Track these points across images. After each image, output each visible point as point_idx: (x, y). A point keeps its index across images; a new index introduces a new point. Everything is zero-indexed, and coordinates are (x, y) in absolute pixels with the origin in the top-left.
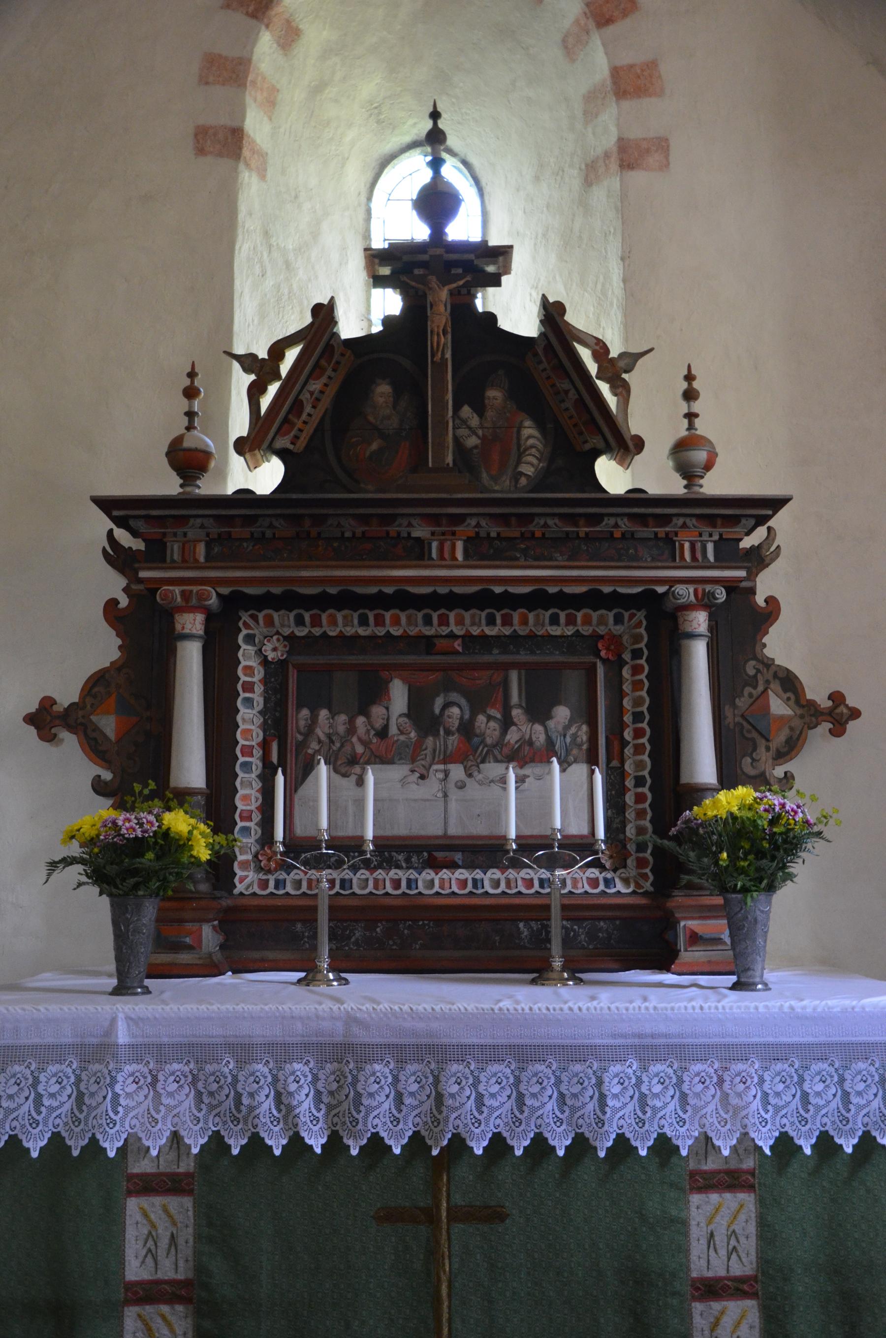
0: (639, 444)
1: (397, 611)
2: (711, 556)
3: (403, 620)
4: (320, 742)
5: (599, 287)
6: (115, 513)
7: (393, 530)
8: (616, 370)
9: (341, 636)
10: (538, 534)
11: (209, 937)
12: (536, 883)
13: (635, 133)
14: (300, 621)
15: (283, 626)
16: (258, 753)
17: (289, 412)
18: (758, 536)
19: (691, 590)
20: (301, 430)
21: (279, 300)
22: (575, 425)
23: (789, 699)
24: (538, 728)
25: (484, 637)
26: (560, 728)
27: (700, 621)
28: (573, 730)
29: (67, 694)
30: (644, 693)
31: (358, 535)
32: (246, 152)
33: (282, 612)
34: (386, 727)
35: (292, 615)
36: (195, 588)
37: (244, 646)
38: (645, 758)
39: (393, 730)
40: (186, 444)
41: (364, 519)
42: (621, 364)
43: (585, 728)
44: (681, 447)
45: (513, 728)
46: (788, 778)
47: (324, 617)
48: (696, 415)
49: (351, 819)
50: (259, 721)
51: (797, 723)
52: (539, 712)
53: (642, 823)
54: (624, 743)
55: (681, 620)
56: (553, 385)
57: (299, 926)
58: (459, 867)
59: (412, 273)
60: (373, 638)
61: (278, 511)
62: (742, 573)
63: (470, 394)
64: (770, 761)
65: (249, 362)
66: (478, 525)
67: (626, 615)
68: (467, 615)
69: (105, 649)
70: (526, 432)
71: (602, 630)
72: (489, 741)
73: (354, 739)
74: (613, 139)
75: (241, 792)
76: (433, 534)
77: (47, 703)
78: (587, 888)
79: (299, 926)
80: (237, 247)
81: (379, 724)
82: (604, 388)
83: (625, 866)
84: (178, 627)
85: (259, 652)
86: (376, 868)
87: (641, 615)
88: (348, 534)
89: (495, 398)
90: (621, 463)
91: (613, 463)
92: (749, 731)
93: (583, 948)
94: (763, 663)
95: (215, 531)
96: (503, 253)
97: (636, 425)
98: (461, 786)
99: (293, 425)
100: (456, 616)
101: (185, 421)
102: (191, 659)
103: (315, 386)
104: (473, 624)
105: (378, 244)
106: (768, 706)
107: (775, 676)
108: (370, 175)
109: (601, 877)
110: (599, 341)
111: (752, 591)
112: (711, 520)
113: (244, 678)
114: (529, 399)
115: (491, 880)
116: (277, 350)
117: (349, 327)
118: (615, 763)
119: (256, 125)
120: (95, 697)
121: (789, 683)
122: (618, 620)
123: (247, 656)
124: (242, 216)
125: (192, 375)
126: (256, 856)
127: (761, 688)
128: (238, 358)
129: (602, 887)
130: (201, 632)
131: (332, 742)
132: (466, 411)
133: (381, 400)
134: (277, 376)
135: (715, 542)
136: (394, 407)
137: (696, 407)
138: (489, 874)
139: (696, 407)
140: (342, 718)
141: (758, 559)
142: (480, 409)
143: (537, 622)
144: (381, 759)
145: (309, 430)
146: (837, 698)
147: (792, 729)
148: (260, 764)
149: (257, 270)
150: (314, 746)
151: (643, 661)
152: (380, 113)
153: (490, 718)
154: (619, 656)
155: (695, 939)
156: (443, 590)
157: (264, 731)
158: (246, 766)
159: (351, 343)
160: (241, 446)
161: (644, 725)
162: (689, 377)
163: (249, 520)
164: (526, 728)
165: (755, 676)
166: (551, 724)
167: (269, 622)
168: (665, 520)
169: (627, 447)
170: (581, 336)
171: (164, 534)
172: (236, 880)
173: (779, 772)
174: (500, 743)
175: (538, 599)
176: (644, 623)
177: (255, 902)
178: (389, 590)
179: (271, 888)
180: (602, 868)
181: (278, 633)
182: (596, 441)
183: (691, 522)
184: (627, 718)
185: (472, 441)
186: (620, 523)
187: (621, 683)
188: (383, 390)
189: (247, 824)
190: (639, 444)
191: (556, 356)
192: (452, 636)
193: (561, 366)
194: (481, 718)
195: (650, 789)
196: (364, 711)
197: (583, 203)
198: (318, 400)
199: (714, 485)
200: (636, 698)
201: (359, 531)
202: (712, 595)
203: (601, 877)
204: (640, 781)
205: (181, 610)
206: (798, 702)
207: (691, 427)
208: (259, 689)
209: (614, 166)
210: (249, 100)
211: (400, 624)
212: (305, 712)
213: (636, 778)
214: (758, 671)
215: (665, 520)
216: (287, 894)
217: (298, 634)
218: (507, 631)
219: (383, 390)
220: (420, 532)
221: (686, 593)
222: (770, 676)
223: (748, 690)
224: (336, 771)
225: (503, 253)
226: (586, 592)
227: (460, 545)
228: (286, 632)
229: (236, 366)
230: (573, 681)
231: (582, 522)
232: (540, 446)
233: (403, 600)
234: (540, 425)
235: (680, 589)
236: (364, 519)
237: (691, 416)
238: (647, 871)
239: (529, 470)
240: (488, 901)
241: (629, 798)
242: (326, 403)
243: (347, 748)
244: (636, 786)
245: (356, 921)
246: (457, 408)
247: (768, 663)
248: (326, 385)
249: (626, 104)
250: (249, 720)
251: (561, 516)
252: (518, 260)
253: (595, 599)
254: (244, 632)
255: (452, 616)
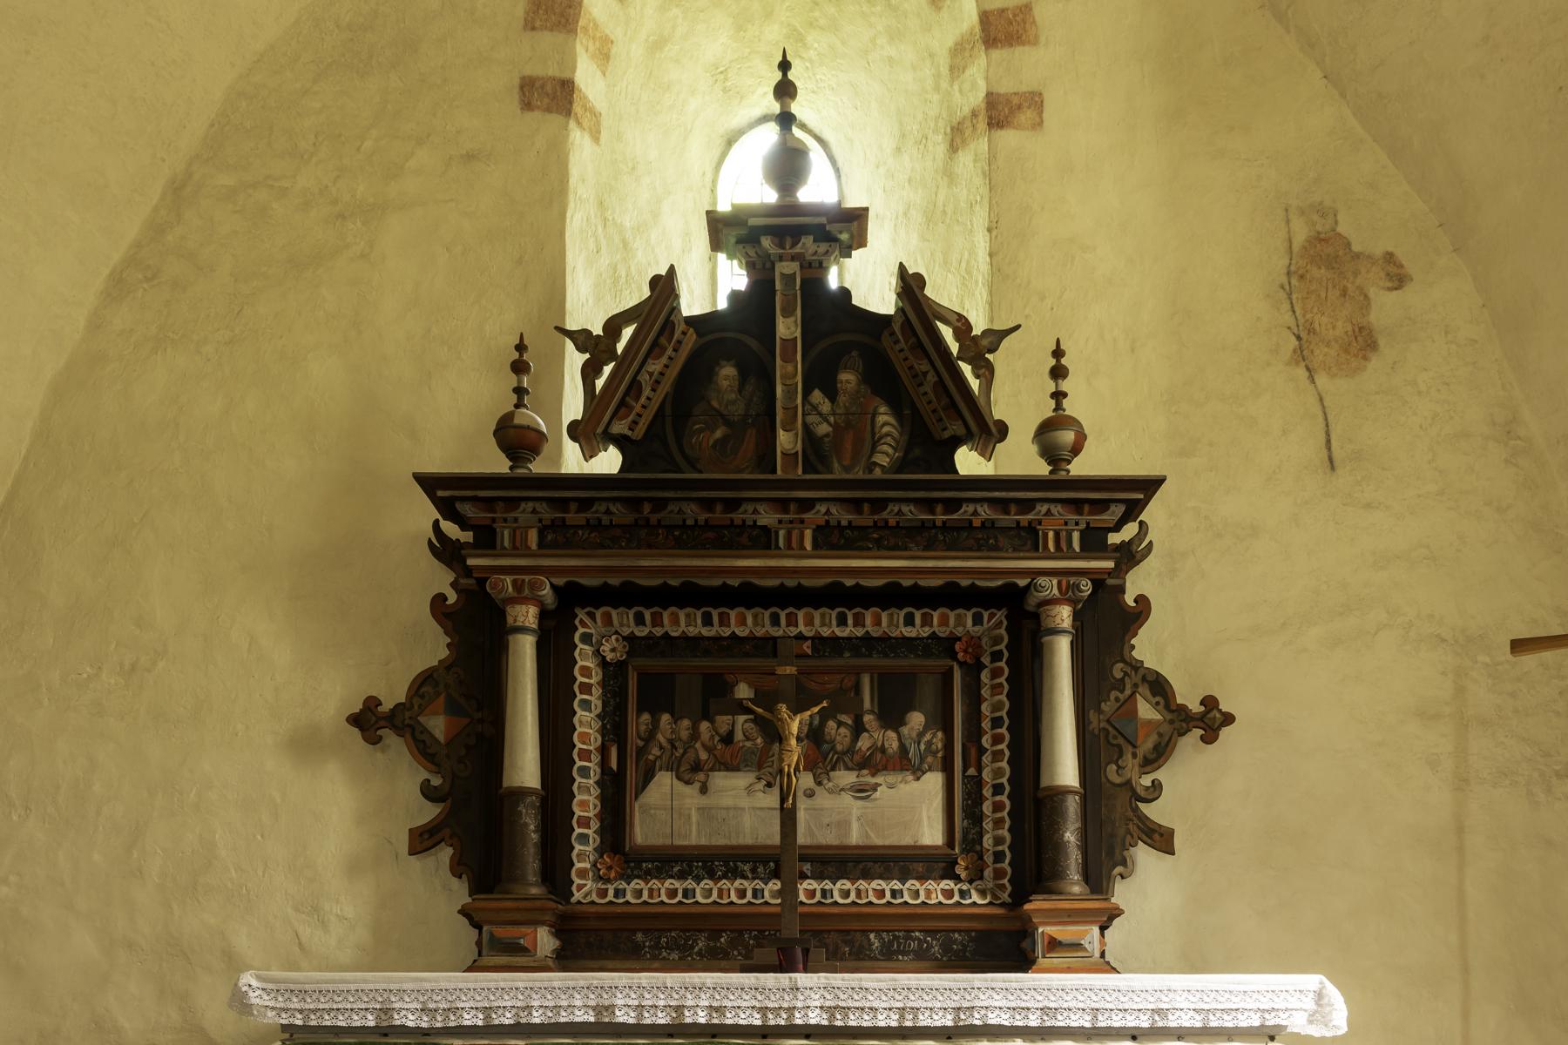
0: (1002, 430)
1: (742, 609)
2: (1076, 546)
3: (750, 620)
4: (661, 748)
5: (964, 265)
6: (440, 493)
7: (737, 517)
8: (981, 348)
9: (685, 638)
10: (892, 522)
11: (545, 941)
12: (888, 894)
13: (1005, 87)
14: (640, 620)
15: (622, 625)
16: (596, 758)
17: (627, 393)
18: (1130, 530)
19: (1055, 582)
20: (639, 415)
21: (616, 280)
22: (934, 411)
23: (1158, 703)
24: (891, 734)
25: (834, 639)
26: (914, 735)
27: (1064, 615)
28: (928, 737)
29: (393, 693)
30: (1003, 697)
31: (701, 523)
32: (577, 108)
33: (621, 609)
34: (731, 733)
35: (631, 614)
36: (527, 578)
37: (581, 646)
38: (1004, 764)
39: (739, 736)
40: (517, 421)
41: (708, 504)
42: (985, 342)
43: (940, 734)
44: (1046, 430)
45: (865, 734)
46: (1157, 787)
47: (666, 615)
48: (1065, 395)
49: (694, 828)
50: (597, 725)
51: (1166, 728)
52: (892, 717)
53: (1000, 832)
54: (982, 751)
55: (1043, 617)
56: (911, 368)
57: (639, 936)
58: (807, 877)
59: (759, 242)
60: (717, 639)
61: (615, 494)
62: (1110, 564)
63: (820, 377)
64: (1137, 768)
65: (582, 339)
66: (828, 512)
67: (986, 615)
68: (817, 614)
69: (434, 648)
70: (881, 419)
71: (959, 631)
72: (839, 748)
73: (698, 745)
74: (982, 94)
75: (579, 798)
76: (780, 522)
77: (372, 703)
78: (941, 898)
79: (639, 936)
80: (568, 215)
81: (724, 729)
82: (966, 369)
83: (981, 878)
84: (510, 620)
85: (597, 652)
86: (720, 878)
87: (1000, 615)
88: (690, 522)
89: (848, 382)
90: (982, 454)
91: (974, 454)
92: (1115, 737)
93: (936, 959)
94: (1130, 665)
95: (548, 514)
96: (856, 218)
97: (999, 411)
98: (810, 794)
99: (631, 408)
100: (806, 615)
101: (514, 398)
102: (524, 653)
103: (655, 366)
104: (823, 624)
105: (724, 207)
106: (1135, 711)
107: (1144, 679)
108: (717, 152)
109: (956, 889)
110: (960, 317)
111: (1121, 589)
112: (1076, 505)
113: (581, 679)
114: (884, 381)
115: (841, 890)
116: (613, 326)
117: (692, 303)
118: (972, 771)
119: (587, 77)
120: (422, 697)
121: (1159, 687)
122: (978, 620)
123: (584, 658)
124: (573, 181)
125: (521, 347)
126: (594, 865)
127: (1128, 692)
128: (570, 334)
129: (957, 898)
130: (535, 626)
131: (674, 747)
132: (817, 396)
133: (725, 383)
134: (612, 355)
135: (1082, 532)
136: (740, 391)
137: (1065, 386)
138: (838, 885)
139: (1065, 386)
140: (686, 723)
141: (1130, 556)
142: (832, 394)
143: (890, 623)
144: (730, 767)
145: (648, 416)
146: (1210, 702)
147: (1160, 735)
148: (599, 770)
149: (592, 246)
150: (656, 751)
151: (1002, 664)
152: (726, 79)
153: (840, 724)
154: (978, 660)
155: (1054, 945)
156: (791, 583)
157: (603, 736)
158: (584, 772)
159: (692, 321)
160: (575, 430)
161: (1004, 730)
162: (1058, 353)
163: (585, 504)
164: (878, 735)
165: (1122, 679)
166: (905, 730)
167: (608, 620)
168: (1027, 506)
169: (990, 434)
170: (943, 312)
171: (494, 520)
172: (574, 889)
173: (1146, 781)
174: (851, 750)
175: (892, 596)
176: (1005, 623)
177: (593, 909)
178: (734, 582)
179: (610, 897)
180: (957, 879)
181: (616, 633)
182: (956, 428)
183: (1056, 509)
184: (986, 725)
185: (823, 429)
186: (980, 509)
187: (979, 689)
188: (727, 373)
189: (585, 831)
190: (1002, 430)
191: (915, 334)
192: (801, 637)
193: (920, 345)
194: (831, 724)
195: (1009, 797)
196: (707, 716)
197: (949, 175)
198: (658, 382)
199: (1079, 467)
200: (995, 701)
201: (702, 517)
202: (1077, 587)
203: (956, 889)
204: (998, 789)
205: (513, 601)
206: (1167, 707)
207: (1059, 407)
208: (597, 691)
209: (982, 124)
210: (579, 49)
211: (746, 623)
212: (646, 717)
213: (994, 786)
214: (1126, 674)
215: (1027, 506)
216: (627, 902)
217: (638, 634)
218: (859, 632)
219: (727, 373)
220: (767, 518)
221: (1050, 587)
222: (1137, 679)
223: (1114, 694)
224: (678, 778)
225: (856, 218)
226: (941, 587)
227: (808, 533)
228: (626, 631)
229: (570, 345)
230: (928, 690)
231: (939, 508)
232: (896, 434)
233: (749, 596)
234: (897, 411)
235: (1042, 581)
236: (708, 504)
237: (1058, 396)
238: (1005, 881)
239: (883, 460)
240: (835, 910)
241: (987, 807)
242: (666, 386)
243: (691, 755)
244: (995, 862)
245: (700, 931)
246: (807, 392)
247: (1137, 666)
248: (666, 366)
249: (997, 54)
250: (586, 724)
251: (916, 501)
252: (875, 230)
253: (953, 596)
254: (581, 630)
255: (801, 615)
